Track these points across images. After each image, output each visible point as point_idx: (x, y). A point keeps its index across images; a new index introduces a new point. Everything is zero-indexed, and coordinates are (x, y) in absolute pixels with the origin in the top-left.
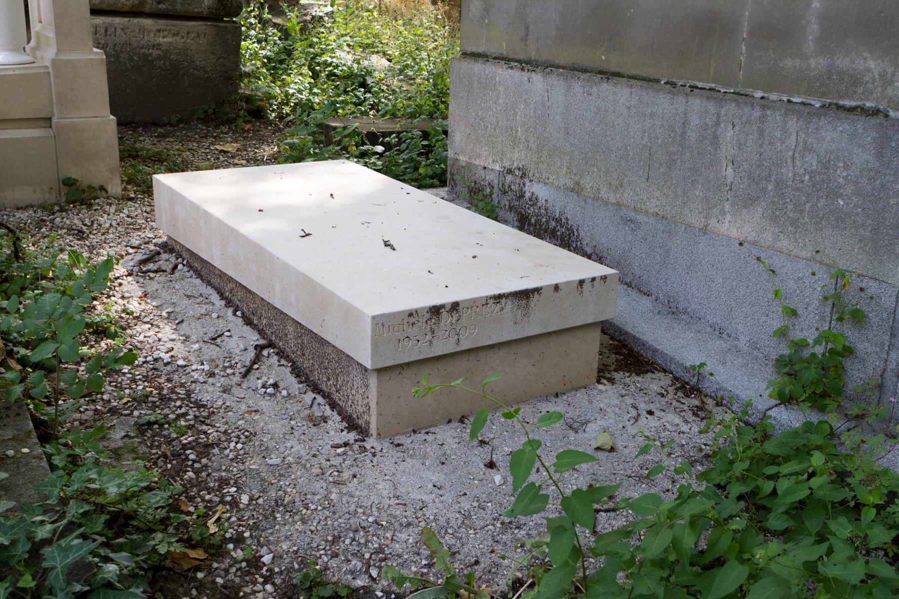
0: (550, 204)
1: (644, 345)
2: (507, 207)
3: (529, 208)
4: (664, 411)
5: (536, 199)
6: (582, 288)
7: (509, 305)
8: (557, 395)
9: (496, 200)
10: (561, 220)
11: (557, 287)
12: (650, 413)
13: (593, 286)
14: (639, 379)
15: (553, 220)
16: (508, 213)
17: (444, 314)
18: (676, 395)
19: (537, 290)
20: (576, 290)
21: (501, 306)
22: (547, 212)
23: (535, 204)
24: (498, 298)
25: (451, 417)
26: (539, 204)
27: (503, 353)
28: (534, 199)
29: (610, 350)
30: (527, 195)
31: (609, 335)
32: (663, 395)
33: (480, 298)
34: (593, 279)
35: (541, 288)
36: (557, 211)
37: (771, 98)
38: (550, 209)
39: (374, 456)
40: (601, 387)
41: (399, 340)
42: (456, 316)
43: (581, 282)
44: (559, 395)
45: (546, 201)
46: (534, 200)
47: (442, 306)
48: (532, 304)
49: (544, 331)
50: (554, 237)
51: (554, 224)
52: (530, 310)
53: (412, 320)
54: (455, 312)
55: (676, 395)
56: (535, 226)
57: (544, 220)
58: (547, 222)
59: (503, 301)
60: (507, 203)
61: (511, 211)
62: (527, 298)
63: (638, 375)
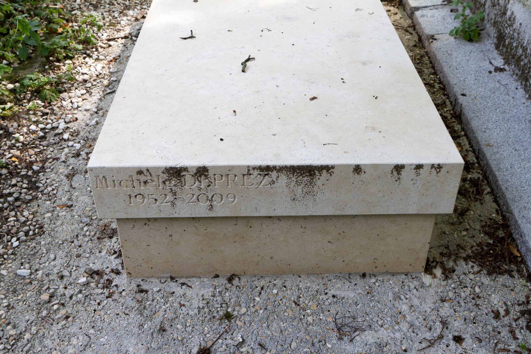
0: (522, 30)
1: (521, 236)
2: (493, 21)
3: (506, 28)
4: (480, 341)
5: (514, 20)
6: (398, 174)
7: (283, 179)
8: (364, 275)
9: (487, 11)
10: (527, 49)
11: (358, 169)
12: (458, 339)
13: (418, 174)
14: (486, 280)
15: (521, 46)
16: (492, 28)
17: (188, 178)
18: (516, 320)
19: (328, 168)
20: (389, 175)
21: (271, 179)
22: (519, 37)
23: (511, 25)
24: (266, 170)
25: (218, 273)
26: (515, 26)
27: (284, 224)
28: (512, 19)
29: (483, 227)
30: (509, 13)
31: (499, 205)
32: (497, 316)
33: (239, 167)
34: (419, 167)
35: (333, 167)
36: (526, 39)
37: (13, 8)
38: (521, 34)
39: (54, 321)
40: (427, 279)
41: (130, 196)
42: (204, 183)
43: (399, 168)
44: (367, 275)
45: (520, 24)
46: (512, 19)
47: (185, 169)
48: (319, 183)
49: (338, 213)
50: (518, 66)
51: (520, 51)
52: (316, 189)
53: (142, 178)
54: (203, 177)
55: (516, 320)
56: (507, 48)
57: (515, 44)
58: (517, 47)
59: (274, 174)
60: (493, 17)
61: (494, 27)
62: (311, 175)
63: (489, 274)
